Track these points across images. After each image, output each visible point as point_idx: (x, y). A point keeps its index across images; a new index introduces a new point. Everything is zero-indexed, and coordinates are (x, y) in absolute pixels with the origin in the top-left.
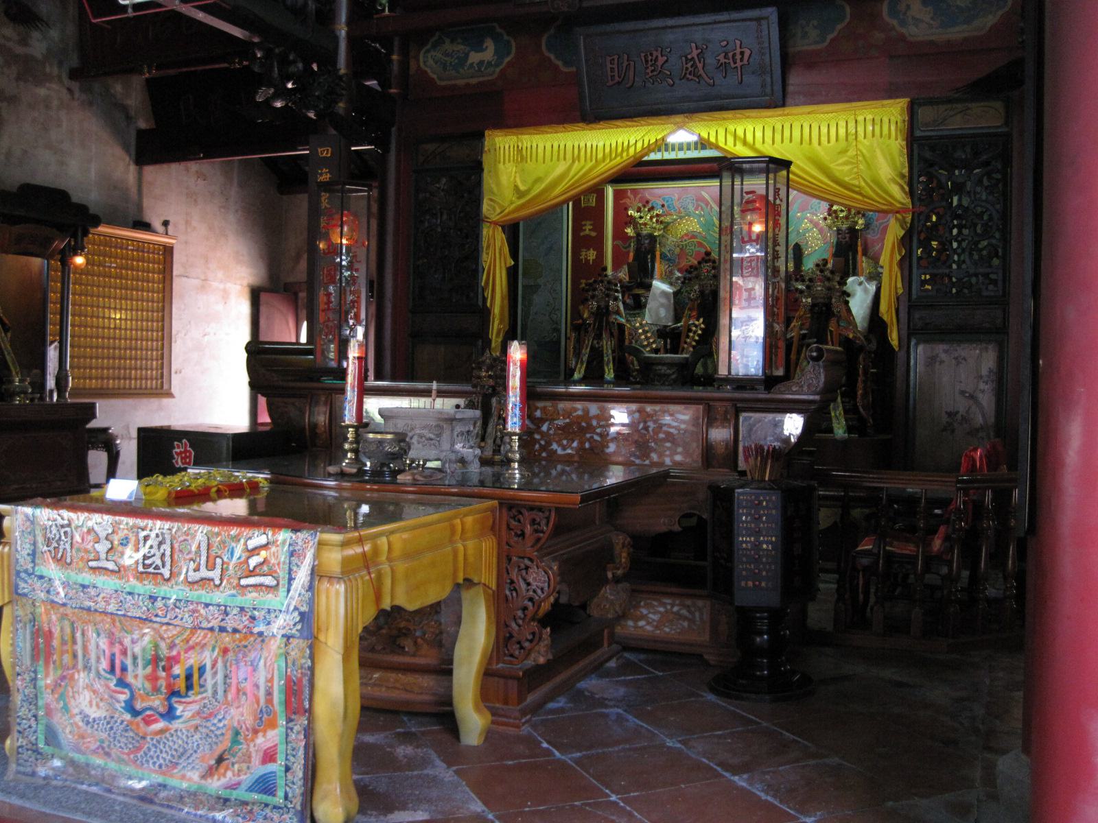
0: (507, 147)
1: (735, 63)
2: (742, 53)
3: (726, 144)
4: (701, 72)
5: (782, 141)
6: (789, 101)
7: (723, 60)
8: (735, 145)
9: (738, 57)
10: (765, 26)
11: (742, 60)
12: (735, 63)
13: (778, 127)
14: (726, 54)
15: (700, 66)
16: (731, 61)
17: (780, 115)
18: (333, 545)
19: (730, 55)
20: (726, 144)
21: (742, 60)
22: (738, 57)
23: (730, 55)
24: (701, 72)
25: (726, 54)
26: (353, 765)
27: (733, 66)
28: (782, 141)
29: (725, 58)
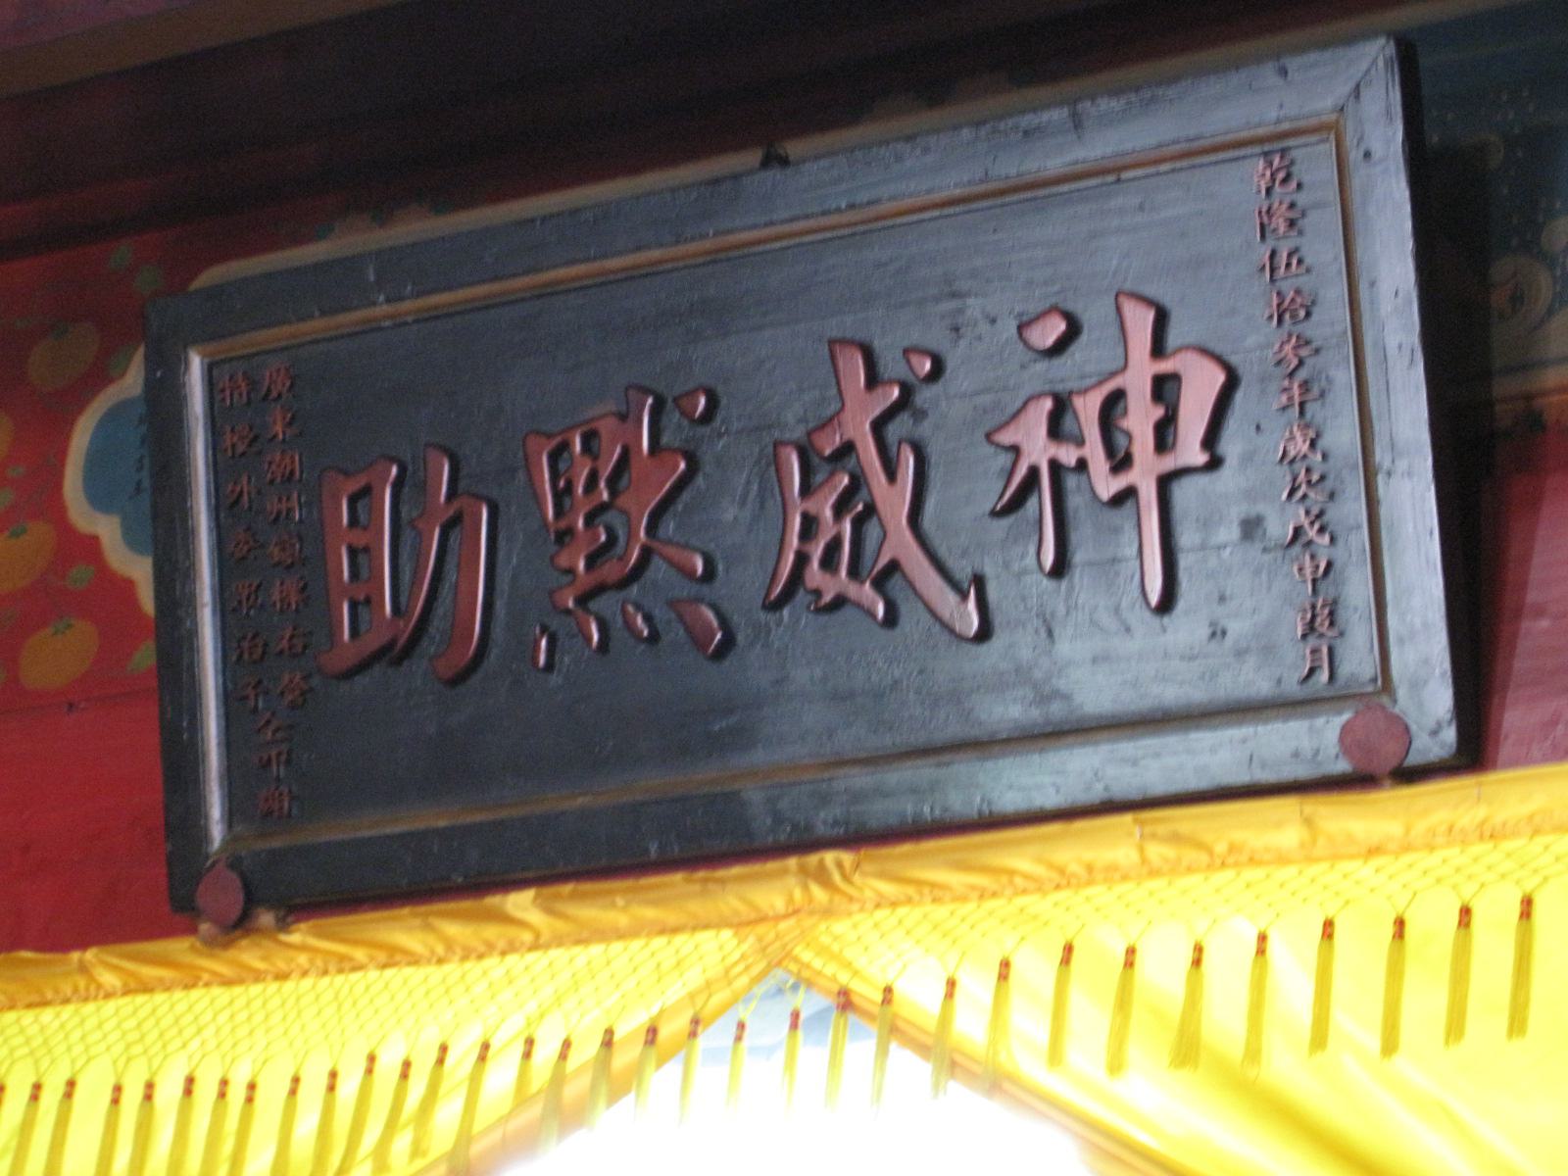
0: (168, 1094)
1: (1121, 462)
2: (1165, 388)
3: (1055, 1054)
4: (901, 544)
5: (1455, 1027)
6: (1514, 718)
7: (1038, 450)
8: (1115, 1065)
9: (1140, 418)
10: (1315, 165)
11: (1164, 435)
12: (1121, 462)
13: (1432, 928)
14: (1061, 406)
15: (893, 500)
16: (1094, 451)
17: (1454, 835)
18: (1196, 717)
19: (1088, 409)
20: (1055, 1054)
21: (1164, 435)
22: (1140, 418)
23: (1088, 409)
24: (901, 544)
25: (1061, 406)
26: (878, 1049)
27: (1107, 486)
28: (1455, 1027)
29: (1055, 431)
